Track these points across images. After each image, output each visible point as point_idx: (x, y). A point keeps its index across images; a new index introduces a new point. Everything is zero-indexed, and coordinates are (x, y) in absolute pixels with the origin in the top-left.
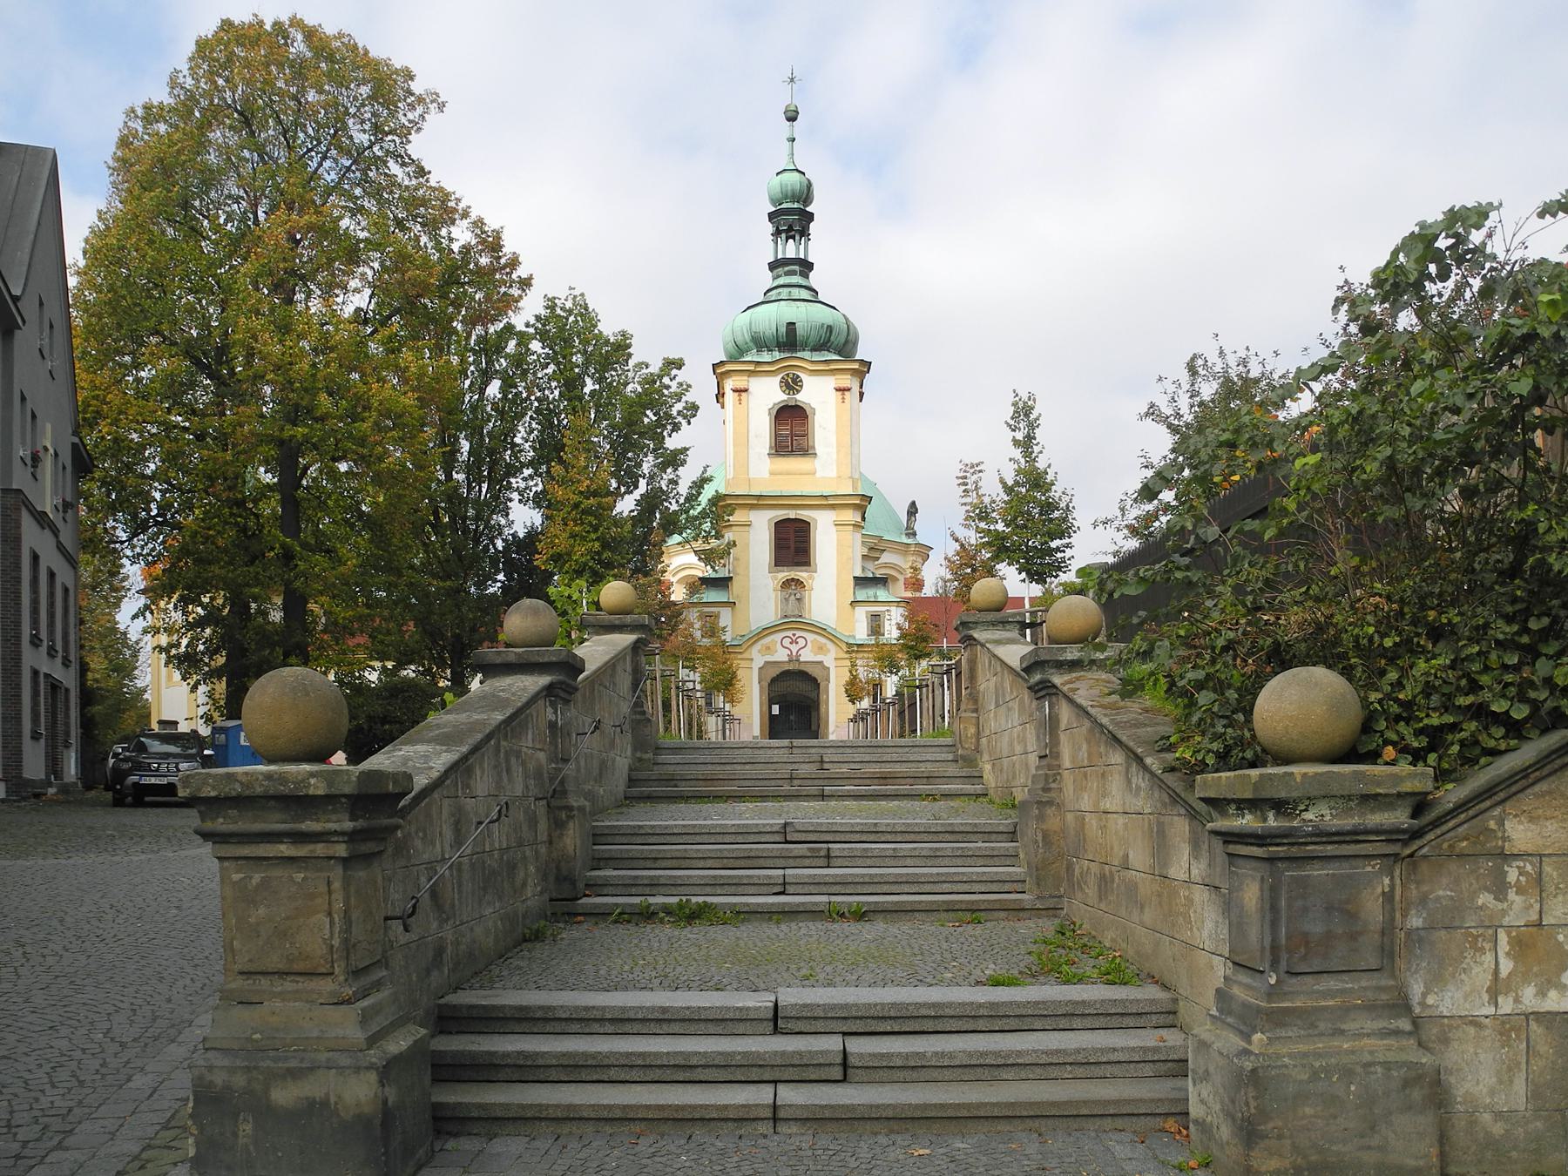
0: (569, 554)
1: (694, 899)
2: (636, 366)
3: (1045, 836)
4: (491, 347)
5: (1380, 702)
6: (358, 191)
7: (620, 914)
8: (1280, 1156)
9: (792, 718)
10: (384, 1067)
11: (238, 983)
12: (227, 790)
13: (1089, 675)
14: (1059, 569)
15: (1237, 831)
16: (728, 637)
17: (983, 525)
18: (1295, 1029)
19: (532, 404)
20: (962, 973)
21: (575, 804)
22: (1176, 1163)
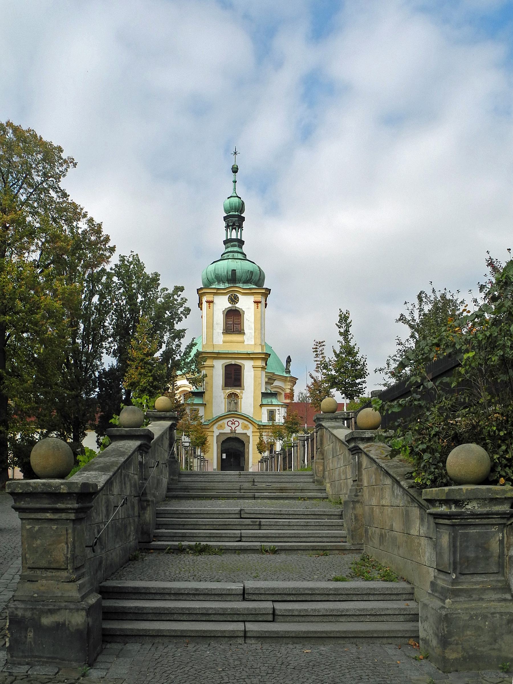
0: (139, 382)
1: (202, 543)
2: (162, 290)
3: (356, 517)
4: (94, 279)
5: (498, 459)
6: (36, 205)
7: (169, 549)
8: (458, 652)
9: (232, 460)
10: (89, 609)
11: (28, 573)
12: (26, 489)
13: (375, 444)
14: (360, 393)
15: (439, 513)
16: (203, 421)
17: (325, 371)
18: (463, 598)
19: (113, 307)
20: (322, 576)
21: (150, 499)
22: (414, 657)
